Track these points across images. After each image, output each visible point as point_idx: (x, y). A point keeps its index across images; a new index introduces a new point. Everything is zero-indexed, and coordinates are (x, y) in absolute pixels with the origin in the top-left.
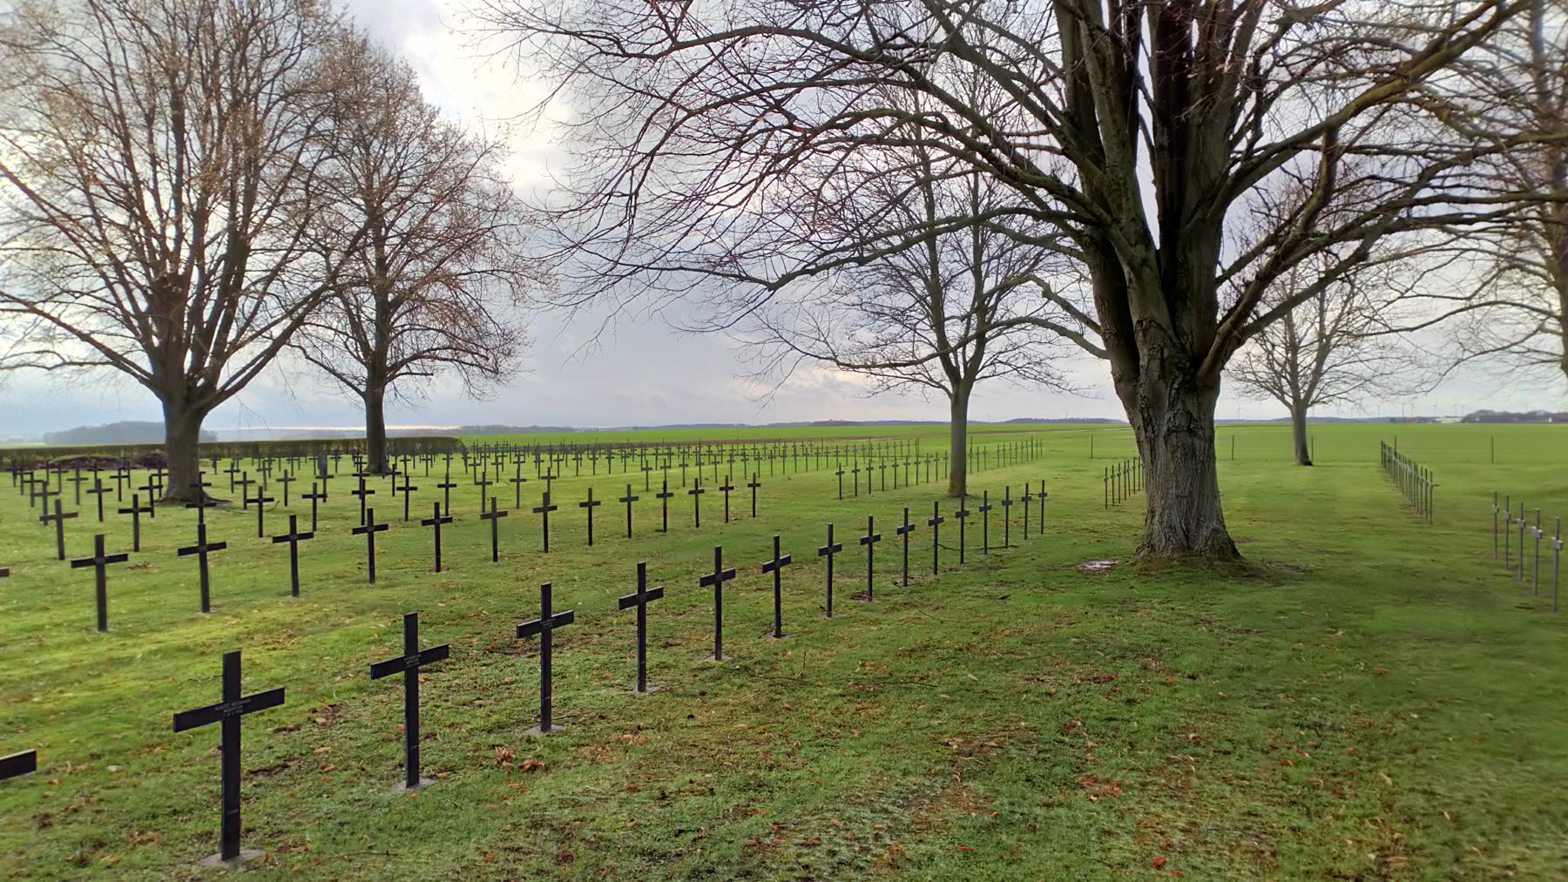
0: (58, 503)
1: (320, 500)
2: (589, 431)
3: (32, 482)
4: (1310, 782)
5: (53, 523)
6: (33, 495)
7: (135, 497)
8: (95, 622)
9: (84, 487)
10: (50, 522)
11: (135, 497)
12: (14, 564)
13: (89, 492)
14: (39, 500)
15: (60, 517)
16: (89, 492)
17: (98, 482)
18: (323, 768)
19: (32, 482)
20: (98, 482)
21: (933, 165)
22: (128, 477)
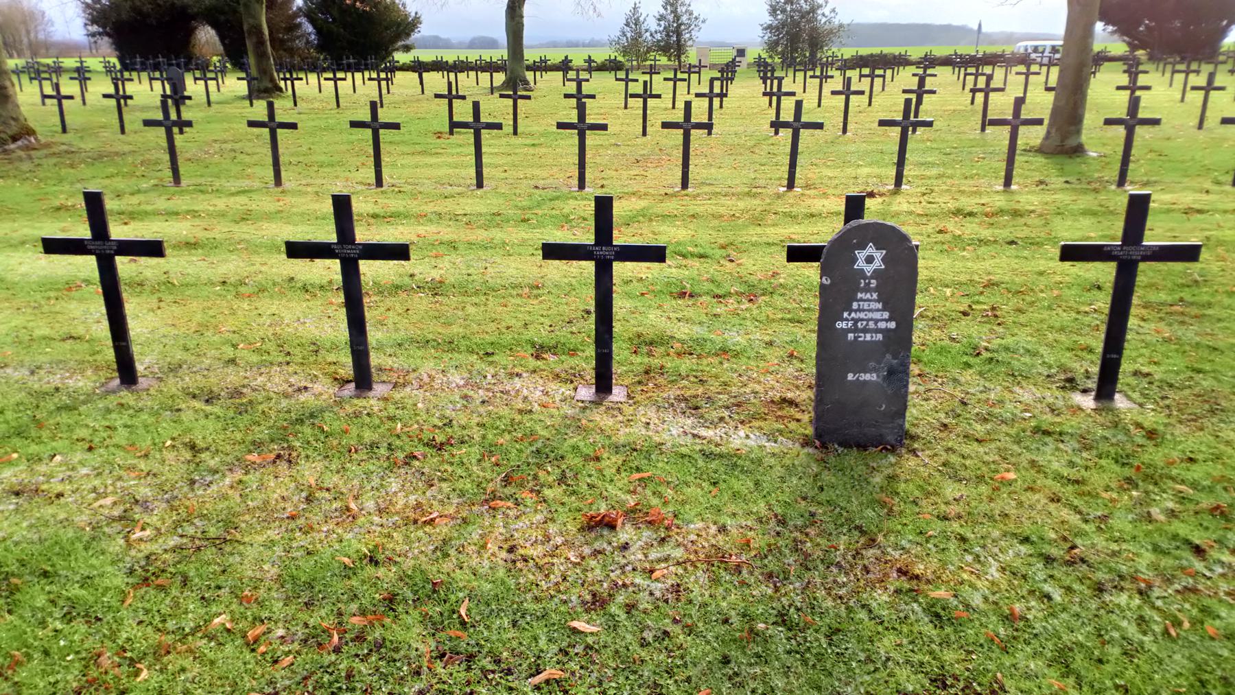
0: (799, 104)
1: (716, 101)
2: (1002, 33)
3: (976, 75)
4: (1175, 617)
5: (785, 134)
6: (974, 91)
7: (688, 105)
8: (373, 181)
9: (829, 87)
10: (782, 132)
11: (688, 105)
12: (674, 195)
13: (834, 93)
14: (980, 97)
15: (797, 126)
16: (834, 93)
17: (848, 82)
18: (89, 505)
19: (976, 75)
20: (848, 82)
21: (532, 73)
22: (883, 76)
